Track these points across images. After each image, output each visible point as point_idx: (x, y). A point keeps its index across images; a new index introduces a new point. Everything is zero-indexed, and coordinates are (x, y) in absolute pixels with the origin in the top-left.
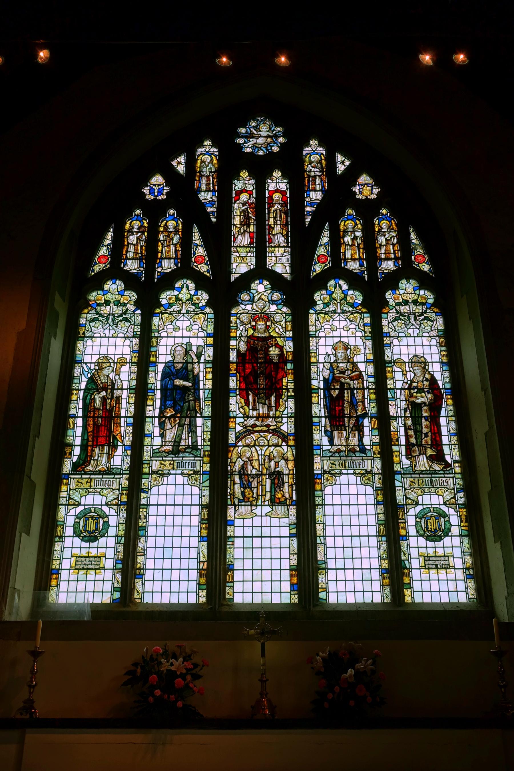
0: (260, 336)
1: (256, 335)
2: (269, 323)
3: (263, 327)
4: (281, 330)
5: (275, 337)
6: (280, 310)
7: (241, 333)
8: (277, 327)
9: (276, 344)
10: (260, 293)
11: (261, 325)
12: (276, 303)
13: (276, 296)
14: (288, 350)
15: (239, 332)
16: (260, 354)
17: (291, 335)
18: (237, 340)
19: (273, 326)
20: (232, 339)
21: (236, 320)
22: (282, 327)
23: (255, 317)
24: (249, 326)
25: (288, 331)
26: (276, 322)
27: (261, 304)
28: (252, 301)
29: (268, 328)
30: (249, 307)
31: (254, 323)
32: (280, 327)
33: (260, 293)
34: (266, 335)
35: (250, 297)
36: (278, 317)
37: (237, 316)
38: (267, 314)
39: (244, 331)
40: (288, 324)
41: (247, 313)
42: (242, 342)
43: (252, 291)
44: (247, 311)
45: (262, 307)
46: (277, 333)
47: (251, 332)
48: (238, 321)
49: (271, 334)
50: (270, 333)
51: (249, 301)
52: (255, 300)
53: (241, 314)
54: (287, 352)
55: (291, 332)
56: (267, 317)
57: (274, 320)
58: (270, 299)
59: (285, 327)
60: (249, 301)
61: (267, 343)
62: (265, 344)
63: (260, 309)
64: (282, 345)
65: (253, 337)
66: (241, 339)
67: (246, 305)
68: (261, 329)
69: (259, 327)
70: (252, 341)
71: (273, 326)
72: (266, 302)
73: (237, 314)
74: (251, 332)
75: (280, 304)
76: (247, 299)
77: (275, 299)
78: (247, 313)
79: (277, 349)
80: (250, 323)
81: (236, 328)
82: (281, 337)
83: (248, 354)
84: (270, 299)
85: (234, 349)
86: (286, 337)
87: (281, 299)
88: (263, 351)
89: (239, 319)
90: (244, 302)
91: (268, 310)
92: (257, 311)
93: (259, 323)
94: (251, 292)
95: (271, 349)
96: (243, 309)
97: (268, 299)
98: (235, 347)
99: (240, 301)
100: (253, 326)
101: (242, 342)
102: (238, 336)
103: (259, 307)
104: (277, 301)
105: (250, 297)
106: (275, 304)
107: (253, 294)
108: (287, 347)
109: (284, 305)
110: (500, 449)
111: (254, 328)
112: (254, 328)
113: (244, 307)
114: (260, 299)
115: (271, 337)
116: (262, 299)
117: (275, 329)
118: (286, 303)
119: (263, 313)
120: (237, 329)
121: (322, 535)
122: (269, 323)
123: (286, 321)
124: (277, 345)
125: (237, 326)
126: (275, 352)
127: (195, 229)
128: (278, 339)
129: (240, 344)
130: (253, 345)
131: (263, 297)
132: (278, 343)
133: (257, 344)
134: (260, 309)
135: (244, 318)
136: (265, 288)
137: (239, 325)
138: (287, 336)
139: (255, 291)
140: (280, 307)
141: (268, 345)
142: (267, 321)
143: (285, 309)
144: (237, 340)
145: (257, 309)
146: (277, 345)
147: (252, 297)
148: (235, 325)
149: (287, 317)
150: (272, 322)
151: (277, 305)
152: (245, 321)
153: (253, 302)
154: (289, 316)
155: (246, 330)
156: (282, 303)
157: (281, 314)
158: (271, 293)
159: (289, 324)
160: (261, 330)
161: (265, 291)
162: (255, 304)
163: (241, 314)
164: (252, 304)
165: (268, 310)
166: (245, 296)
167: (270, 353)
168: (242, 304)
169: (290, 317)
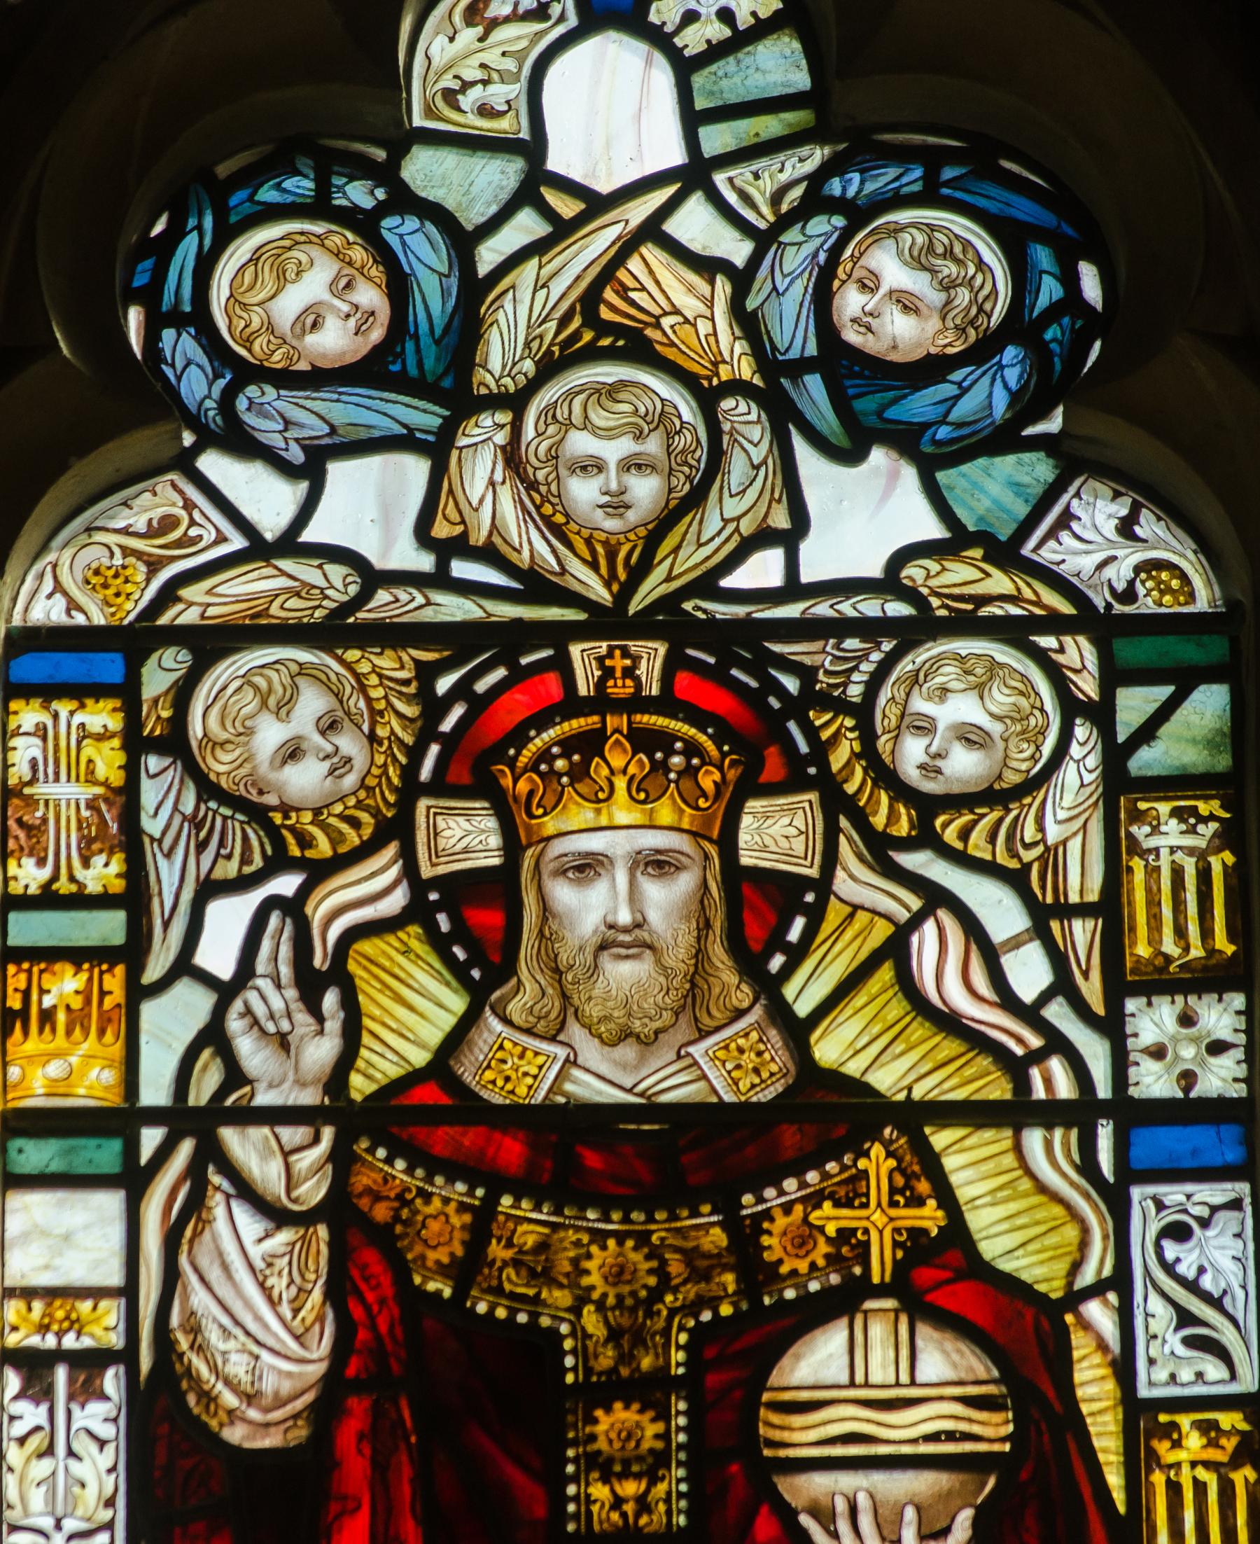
0: (588, 1088)
1: (518, 1066)
2: (776, 832)
3: (663, 900)
4: (1029, 973)
5: (916, 1116)
6: (1005, 553)
7: (213, 1036)
8: (936, 898)
9: (915, 1246)
10: (598, 205)
11: (617, 873)
12: (919, 405)
13: (910, 285)
14: (1168, 1366)
15: (172, 1020)
16: (606, 1469)
17: (1221, 1078)
18: (133, 1180)
19: (856, 881)
20: (33, 1154)
21: (108, 762)
22: (1045, 918)
23: (491, 697)
24: (374, 887)
25: (1161, 981)
26: (927, 807)
27: (607, 454)
28: (427, 372)
29: (759, 918)
30: (369, 507)
31: (465, 836)
32: (1001, 912)
33: (598, 205)
34: (725, 1068)
35: (399, 286)
36: (963, 709)
37: (127, 693)
38: (747, 640)
39: (272, 996)
40: (1169, 837)
41: (334, 631)
42: (235, 1230)
43: (426, 171)
44: (339, 582)
45: (646, 492)
46: (948, 1022)
47: (413, 1011)
48: (162, 795)
49: (829, 1049)
50: (798, 1032)
51: (369, 372)
52: (501, 355)
53: (210, 643)
54: (1143, 1419)
55: (1220, 1016)
56: (750, 699)
57: (885, 776)
58: (792, 330)
59: (1110, 908)
60: (369, 372)
61: (746, 1235)
62: (701, 1266)
63: (601, 552)
64: (1040, 1271)
65: (470, 1108)
66: (211, 1153)
67: (310, 470)
68: (610, 942)
69: (586, 908)
70: (445, 1207)
71: (856, 881)
72: (708, 398)
73: (136, 641)
74: (413, 1011)
75: (1002, 439)
76: (334, 341)
77: (903, 334)
78: (334, 631)
79: (942, 1359)
80: (396, 829)
81: (109, 927)
82: (1017, 1113)
83: (354, 1467)
84: (792, 330)
85: (89, 1363)
86: (1132, 1113)
87: (1019, 326)
88: (650, 1392)
89: (174, 742)
90: (265, 411)
91: (764, 570)
92: (536, 586)
93: (573, 826)
94: (404, 200)
95: (819, 1359)
96: (259, 550)
97: (749, 325)
98: (104, 1326)
99: (197, 386)
100: (464, 888)
101: (235, 1230)
102: (155, 1091)
103: (583, 493)
104: (931, 369)
105: (399, 286)
106: (906, 440)
107: (462, 242)
108: (1155, 1313)
109: (1073, 461)
110: (551, 249)
111: (479, 925)
112: (479, 925)
113: (267, 499)
114: (602, 331)
115: (831, 1115)
116: (637, 347)
117: (896, 949)
118: (1089, 391)
119: (666, 620)
120: (133, 951)
121: (249, 693)
122: (776, 832)
123: (1120, 787)
124: (943, 1279)
125: (134, 897)
126: (903, 1429)
127: (1122, 1509)
128: (968, 1158)
129: (198, 1256)
130: (467, 1270)
131: (661, 284)
132: (957, 1230)
133: (537, 1263)
134: (601, 552)
135: (270, 735)
136: (692, 120)
137: (169, 877)
138: (1152, 1081)
139: (501, 175)
140: (995, 487)
141: (756, 1272)
142: (750, 785)
143: (1099, 541)
144: (133, 1180)
145: (535, 547)
146: (943, 1279)
147: (433, 296)
148: (104, 873)
149: (1134, 704)
150: (836, 803)
151: (931, 457)
152: (305, 780)
153: (462, 402)
154: (1184, 681)
155: (310, 985)
156: (1029, 404)
157: (1015, 632)
158: (815, 200)
159: (1172, 838)
160: (624, 974)
161: (695, 175)
162: (486, 429)
163: (210, 643)
164: (438, 450)
165: (764, 570)
166: (298, 290)
167: (804, 1435)
168: (242, 444)
169: (1209, 705)
